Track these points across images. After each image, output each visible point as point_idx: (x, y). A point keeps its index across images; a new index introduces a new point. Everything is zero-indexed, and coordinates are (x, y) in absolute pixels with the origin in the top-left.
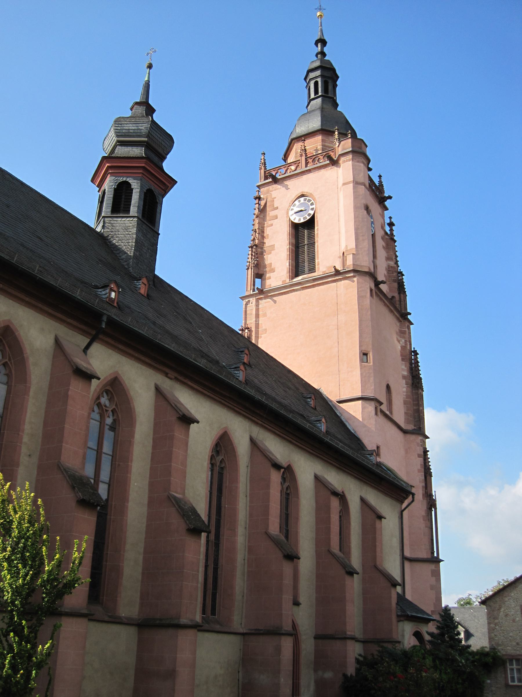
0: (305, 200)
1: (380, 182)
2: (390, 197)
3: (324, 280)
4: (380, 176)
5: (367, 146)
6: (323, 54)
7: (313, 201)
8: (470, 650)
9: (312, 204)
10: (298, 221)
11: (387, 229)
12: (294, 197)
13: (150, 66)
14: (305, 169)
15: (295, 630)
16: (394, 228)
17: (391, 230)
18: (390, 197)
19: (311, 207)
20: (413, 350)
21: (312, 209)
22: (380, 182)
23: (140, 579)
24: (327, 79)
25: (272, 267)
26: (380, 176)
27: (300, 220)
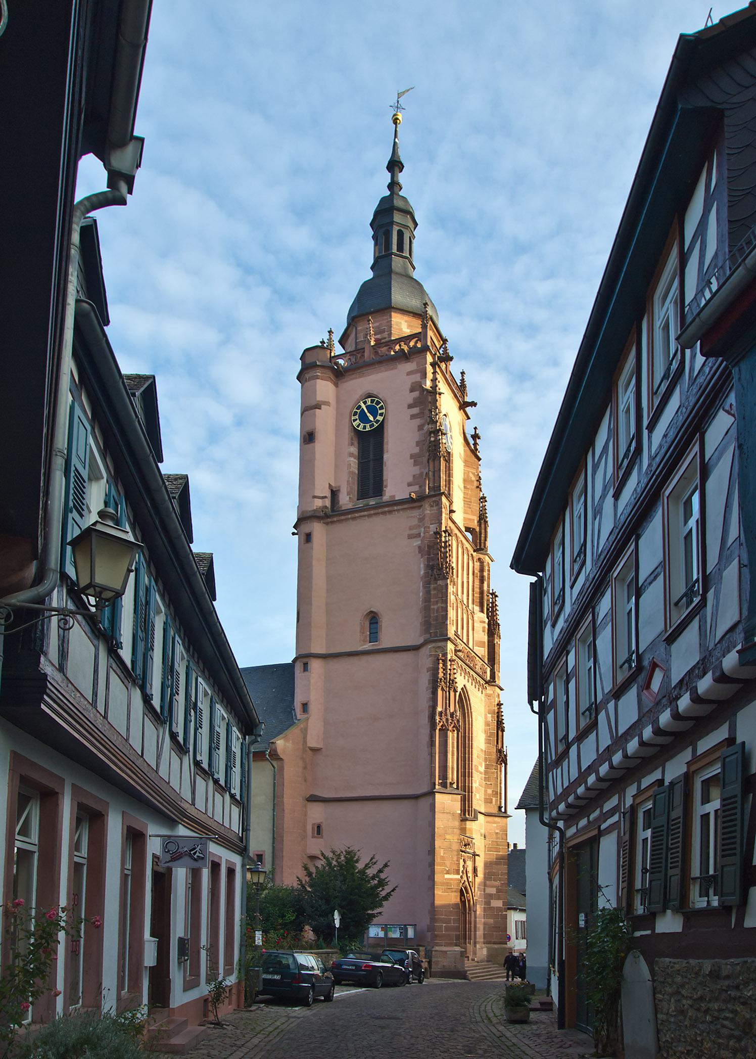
0: (372, 401)
1: (463, 380)
4: (463, 373)
5: (414, 268)
6: (394, 185)
9: (381, 408)
11: (471, 442)
12: (357, 396)
15: (656, 573)
17: (475, 444)
19: (380, 412)
20: (491, 592)
21: (381, 415)
22: (463, 380)
24: (402, 229)
25: (420, 554)
26: (463, 373)
27: (365, 427)
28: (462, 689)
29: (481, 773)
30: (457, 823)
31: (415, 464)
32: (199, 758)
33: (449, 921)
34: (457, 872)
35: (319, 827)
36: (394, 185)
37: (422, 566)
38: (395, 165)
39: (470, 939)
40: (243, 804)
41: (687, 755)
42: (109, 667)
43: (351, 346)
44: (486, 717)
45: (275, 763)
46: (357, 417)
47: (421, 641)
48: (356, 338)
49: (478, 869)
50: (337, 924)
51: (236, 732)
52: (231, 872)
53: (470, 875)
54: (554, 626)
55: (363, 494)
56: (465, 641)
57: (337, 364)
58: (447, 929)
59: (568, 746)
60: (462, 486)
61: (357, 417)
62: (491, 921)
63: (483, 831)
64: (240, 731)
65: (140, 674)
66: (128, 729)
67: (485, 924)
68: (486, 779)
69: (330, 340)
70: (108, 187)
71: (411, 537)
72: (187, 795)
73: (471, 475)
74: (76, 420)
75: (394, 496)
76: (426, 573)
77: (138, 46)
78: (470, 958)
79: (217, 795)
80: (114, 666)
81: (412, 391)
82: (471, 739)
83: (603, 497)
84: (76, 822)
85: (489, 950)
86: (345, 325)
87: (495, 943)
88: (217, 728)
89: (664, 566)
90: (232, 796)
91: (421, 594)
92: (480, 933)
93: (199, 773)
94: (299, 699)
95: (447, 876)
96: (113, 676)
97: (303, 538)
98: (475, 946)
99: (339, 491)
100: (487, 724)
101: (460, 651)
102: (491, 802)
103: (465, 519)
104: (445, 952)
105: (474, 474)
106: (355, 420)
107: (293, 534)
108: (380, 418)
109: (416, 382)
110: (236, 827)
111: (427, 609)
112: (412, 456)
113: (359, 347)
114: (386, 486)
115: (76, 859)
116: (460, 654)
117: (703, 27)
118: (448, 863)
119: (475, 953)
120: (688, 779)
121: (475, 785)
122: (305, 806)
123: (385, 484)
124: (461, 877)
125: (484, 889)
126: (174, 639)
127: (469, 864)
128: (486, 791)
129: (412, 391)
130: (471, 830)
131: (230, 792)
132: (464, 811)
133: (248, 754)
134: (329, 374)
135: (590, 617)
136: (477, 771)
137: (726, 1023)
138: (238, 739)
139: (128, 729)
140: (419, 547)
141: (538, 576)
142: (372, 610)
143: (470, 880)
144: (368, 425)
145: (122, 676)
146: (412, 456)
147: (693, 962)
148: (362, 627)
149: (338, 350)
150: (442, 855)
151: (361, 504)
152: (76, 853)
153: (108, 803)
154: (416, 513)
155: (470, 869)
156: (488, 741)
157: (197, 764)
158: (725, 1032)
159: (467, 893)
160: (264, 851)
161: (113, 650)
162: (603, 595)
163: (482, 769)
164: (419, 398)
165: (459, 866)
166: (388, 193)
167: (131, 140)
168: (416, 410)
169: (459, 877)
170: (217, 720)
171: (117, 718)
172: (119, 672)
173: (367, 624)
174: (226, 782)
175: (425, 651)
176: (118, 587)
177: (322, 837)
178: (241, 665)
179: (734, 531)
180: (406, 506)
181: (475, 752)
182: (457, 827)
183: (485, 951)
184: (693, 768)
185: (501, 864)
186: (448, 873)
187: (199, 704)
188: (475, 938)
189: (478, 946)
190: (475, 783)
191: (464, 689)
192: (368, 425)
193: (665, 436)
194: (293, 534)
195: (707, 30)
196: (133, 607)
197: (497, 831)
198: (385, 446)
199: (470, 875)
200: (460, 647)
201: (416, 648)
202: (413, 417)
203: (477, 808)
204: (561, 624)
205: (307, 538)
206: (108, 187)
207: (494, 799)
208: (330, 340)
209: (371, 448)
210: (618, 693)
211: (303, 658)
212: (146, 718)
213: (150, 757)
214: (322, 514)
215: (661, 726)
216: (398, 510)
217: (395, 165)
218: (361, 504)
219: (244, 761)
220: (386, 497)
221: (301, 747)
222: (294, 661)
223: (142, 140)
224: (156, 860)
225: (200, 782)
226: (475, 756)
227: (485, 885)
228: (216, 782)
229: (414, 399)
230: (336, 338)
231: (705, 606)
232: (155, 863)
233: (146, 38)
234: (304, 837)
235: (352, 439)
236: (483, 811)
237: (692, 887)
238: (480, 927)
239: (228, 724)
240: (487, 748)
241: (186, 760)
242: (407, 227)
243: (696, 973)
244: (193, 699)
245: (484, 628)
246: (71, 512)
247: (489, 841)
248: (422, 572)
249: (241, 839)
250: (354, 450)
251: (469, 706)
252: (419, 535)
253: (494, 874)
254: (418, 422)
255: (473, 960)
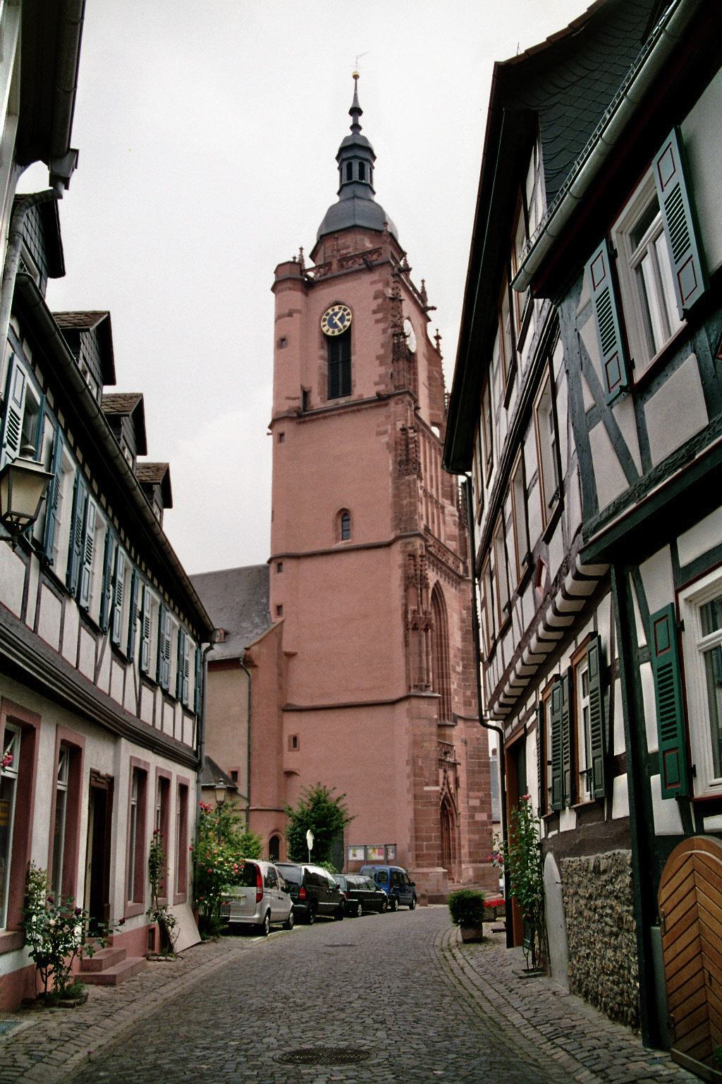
2: (433, 308)
3: (360, 406)
4: (423, 281)
6: (356, 127)
7: (349, 310)
8: (50, 567)
9: (348, 314)
10: (651, 357)
12: (327, 304)
13: (356, 77)
14: (336, 273)
16: (440, 341)
17: (438, 344)
18: (433, 308)
21: (348, 320)
23: (41, 733)
26: (423, 281)
27: (333, 332)
28: (435, 585)
29: (458, 673)
30: (434, 729)
31: (381, 364)
32: (144, 668)
33: (429, 839)
34: (437, 783)
35: (295, 739)
36: (356, 127)
37: (390, 461)
38: (356, 111)
39: (455, 858)
40: (197, 716)
41: (571, 649)
42: (41, 583)
43: (321, 262)
44: (461, 613)
45: (250, 671)
46: (326, 323)
47: (392, 537)
48: (325, 254)
49: (460, 779)
50: (310, 846)
51: (189, 640)
52: (183, 790)
53: (452, 786)
54: (479, 524)
55: (333, 394)
56: (436, 535)
57: (307, 276)
58: (428, 847)
59: (495, 645)
60: (427, 383)
61: (326, 323)
62: (476, 837)
63: (463, 736)
64: (195, 638)
65: (74, 588)
66: (61, 642)
67: (470, 841)
68: (464, 680)
69: (301, 256)
70: (50, 185)
71: (379, 434)
72: (131, 706)
73: (435, 373)
74: (14, 367)
75: (362, 395)
76: (394, 469)
77: (70, 92)
78: (455, 880)
79: (167, 706)
80: (47, 581)
81: (376, 298)
82: (447, 638)
83: (499, 406)
84: (72, 743)
85: (475, 869)
86: (315, 242)
87: (481, 862)
88: (167, 637)
89: (540, 473)
90: (185, 708)
91: (390, 490)
92: (465, 851)
93: (145, 683)
94: (274, 600)
95: (426, 788)
96: (45, 591)
97: (277, 437)
98: (461, 866)
99: (310, 391)
100: (463, 621)
101: (430, 546)
102: (470, 705)
103: (431, 415)
104: (427, 874)
105: (437, 372)
106: (324, 326)
107: (268, 434)
108: (348, 324)
109: (379, 290)
110: (189, 740)
111: (397, 504)
112: (378, 357)
113: (328, 261)
114: (355, 385)
115: (59, 787)
116: (430, 549)
117: (515, 55)
118: (427, 774)
119: (460, 875)
120: (572, 671)
121: (453, 687)
122: (281, 717)
123: (353, 384)
124: (443, 789)
125: (468, 802)
126: (117, 550)
127: (450, 774)
128: (464, 693)
129: (376, 298)
130: (451, 737)
131: (182, 703)
132: (442, 715)
133: (203, 663)
134: (299, 285)
135: (501, 518)
136: (454, 671)
137: (608, 919)
138: (192, 647)
139: (61, 642)
140: (387, 444)
141: (467, 476)
142: (344, 506)
143: (452, 791)
144: (336, 330)
145: (55, 590)
146: (378, 357)
147: (583, 858)
148: (336, 525)
149: (309, 264)
150: (420, 764)
151: (331, 403)
152: (59, 782)
153: (40, 717)
154: (383, 411)
155: (451, 779)
156: (464, 639)
157: (143, 675)
158: (607, 929)
159: (450, 806)
160: (239, 768)
161: (45, 567)
162: (507, 496)
163: (459, 669)
164: (382, 304)
165: (438, 777)
166: (350, 133)
167: (68, 152)
168: (380, 316)
169: (438, 788)
170: (167, 629)
171: (48, 632)
172: (52, 586)
173: (340, 522)
174: (177, 692)
175: (397, 547)
176: (32, 514)
177: (298, 750)
178: (188, 573)
179: (573, 447)
180: (373, 405)
181: (452, 652)
182: (435, 733)
183: (471, 873)
184: (575, 662)
185: (483, 772)
186: (427, 785)
187: (146, 614)
188: (460, 857)
189: (463, 866)
190: (453, 683)
191: (437, 584)
192: (336, 330)
193: (529, 358)
194: (268, 434)
195: (518, 57)
196: (70, 523)
197: (478, 736)
198: (352, 349)
199: (452, 786)
200: (431, 542)
201: (388, 545)
202: (377, 321)
203: (458, 713)
204: (484, 522)
205: (281, 437)
206: (50, 185)
207: (473, 701)
208: (301, 256)
209: (340, 351)
210: (521, 591)
211: (278, 560)
212: (83, 631)
213: (87, 669)
214: (295, 415)
215: (548, 622)
216: (366, 409)
217: (356, 111)
218: (331, 403)
219: (198, 670)
220: (354, 397)
221: (276, 652)
222: (270, 562)
223: (76, 151)
224: (95, 776)
225: (147, 693)
226: (452, 656)
227: (468, 797)
228: (165, 692)
229: (378, 306)
230: (307, 253)
231: (563, 509)
232: (93, 779)
233: (76, 86)
234: (280, 751)
235: (322, 343)
236: (462, 715)
237: (580, 782)
238: (465, 843)
239: (179, 632)
240: (464, 646)
241: (130, 670)
242: (367, 160)
243: (586, 871)
244: (139, 608)
245: (454, 521)
246: (5, 446)
247: (470, 748)
248: (391, 468)
249: (196, 753)
250: (324, 353)
251: (443, 602)
252: (385, 432)
253: (478, 784)
254: (382, 326)
255: (458, 882)
